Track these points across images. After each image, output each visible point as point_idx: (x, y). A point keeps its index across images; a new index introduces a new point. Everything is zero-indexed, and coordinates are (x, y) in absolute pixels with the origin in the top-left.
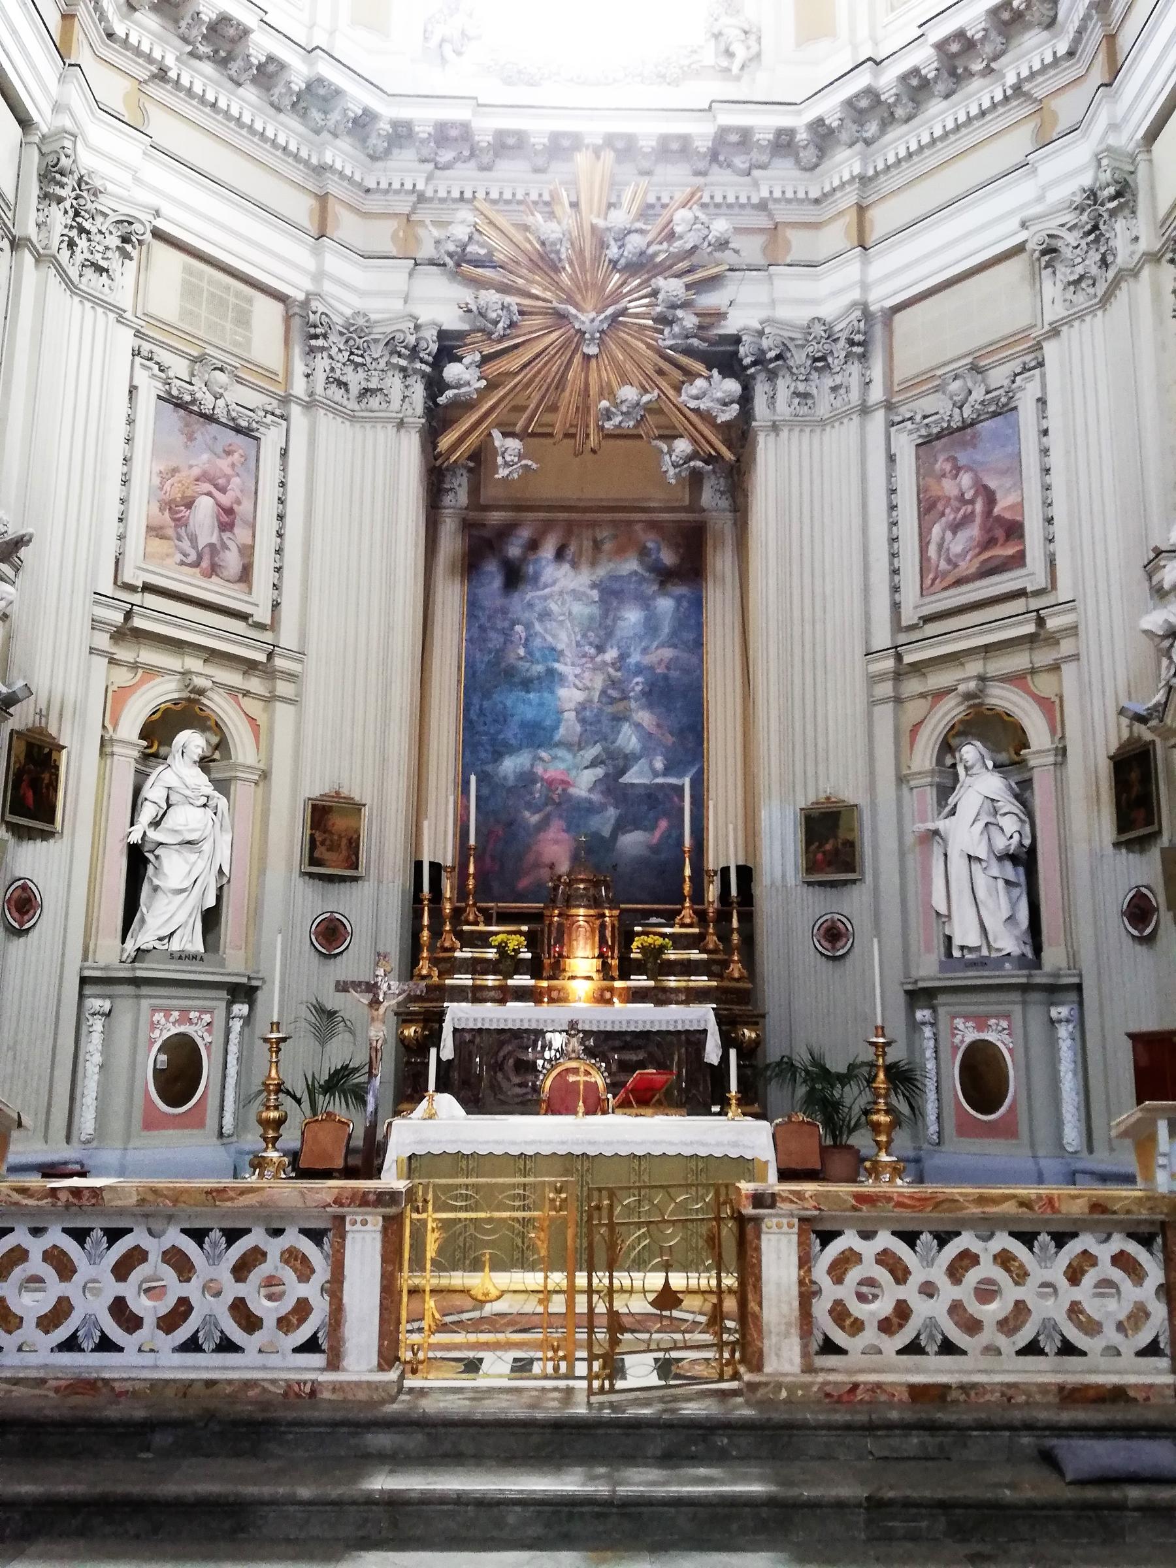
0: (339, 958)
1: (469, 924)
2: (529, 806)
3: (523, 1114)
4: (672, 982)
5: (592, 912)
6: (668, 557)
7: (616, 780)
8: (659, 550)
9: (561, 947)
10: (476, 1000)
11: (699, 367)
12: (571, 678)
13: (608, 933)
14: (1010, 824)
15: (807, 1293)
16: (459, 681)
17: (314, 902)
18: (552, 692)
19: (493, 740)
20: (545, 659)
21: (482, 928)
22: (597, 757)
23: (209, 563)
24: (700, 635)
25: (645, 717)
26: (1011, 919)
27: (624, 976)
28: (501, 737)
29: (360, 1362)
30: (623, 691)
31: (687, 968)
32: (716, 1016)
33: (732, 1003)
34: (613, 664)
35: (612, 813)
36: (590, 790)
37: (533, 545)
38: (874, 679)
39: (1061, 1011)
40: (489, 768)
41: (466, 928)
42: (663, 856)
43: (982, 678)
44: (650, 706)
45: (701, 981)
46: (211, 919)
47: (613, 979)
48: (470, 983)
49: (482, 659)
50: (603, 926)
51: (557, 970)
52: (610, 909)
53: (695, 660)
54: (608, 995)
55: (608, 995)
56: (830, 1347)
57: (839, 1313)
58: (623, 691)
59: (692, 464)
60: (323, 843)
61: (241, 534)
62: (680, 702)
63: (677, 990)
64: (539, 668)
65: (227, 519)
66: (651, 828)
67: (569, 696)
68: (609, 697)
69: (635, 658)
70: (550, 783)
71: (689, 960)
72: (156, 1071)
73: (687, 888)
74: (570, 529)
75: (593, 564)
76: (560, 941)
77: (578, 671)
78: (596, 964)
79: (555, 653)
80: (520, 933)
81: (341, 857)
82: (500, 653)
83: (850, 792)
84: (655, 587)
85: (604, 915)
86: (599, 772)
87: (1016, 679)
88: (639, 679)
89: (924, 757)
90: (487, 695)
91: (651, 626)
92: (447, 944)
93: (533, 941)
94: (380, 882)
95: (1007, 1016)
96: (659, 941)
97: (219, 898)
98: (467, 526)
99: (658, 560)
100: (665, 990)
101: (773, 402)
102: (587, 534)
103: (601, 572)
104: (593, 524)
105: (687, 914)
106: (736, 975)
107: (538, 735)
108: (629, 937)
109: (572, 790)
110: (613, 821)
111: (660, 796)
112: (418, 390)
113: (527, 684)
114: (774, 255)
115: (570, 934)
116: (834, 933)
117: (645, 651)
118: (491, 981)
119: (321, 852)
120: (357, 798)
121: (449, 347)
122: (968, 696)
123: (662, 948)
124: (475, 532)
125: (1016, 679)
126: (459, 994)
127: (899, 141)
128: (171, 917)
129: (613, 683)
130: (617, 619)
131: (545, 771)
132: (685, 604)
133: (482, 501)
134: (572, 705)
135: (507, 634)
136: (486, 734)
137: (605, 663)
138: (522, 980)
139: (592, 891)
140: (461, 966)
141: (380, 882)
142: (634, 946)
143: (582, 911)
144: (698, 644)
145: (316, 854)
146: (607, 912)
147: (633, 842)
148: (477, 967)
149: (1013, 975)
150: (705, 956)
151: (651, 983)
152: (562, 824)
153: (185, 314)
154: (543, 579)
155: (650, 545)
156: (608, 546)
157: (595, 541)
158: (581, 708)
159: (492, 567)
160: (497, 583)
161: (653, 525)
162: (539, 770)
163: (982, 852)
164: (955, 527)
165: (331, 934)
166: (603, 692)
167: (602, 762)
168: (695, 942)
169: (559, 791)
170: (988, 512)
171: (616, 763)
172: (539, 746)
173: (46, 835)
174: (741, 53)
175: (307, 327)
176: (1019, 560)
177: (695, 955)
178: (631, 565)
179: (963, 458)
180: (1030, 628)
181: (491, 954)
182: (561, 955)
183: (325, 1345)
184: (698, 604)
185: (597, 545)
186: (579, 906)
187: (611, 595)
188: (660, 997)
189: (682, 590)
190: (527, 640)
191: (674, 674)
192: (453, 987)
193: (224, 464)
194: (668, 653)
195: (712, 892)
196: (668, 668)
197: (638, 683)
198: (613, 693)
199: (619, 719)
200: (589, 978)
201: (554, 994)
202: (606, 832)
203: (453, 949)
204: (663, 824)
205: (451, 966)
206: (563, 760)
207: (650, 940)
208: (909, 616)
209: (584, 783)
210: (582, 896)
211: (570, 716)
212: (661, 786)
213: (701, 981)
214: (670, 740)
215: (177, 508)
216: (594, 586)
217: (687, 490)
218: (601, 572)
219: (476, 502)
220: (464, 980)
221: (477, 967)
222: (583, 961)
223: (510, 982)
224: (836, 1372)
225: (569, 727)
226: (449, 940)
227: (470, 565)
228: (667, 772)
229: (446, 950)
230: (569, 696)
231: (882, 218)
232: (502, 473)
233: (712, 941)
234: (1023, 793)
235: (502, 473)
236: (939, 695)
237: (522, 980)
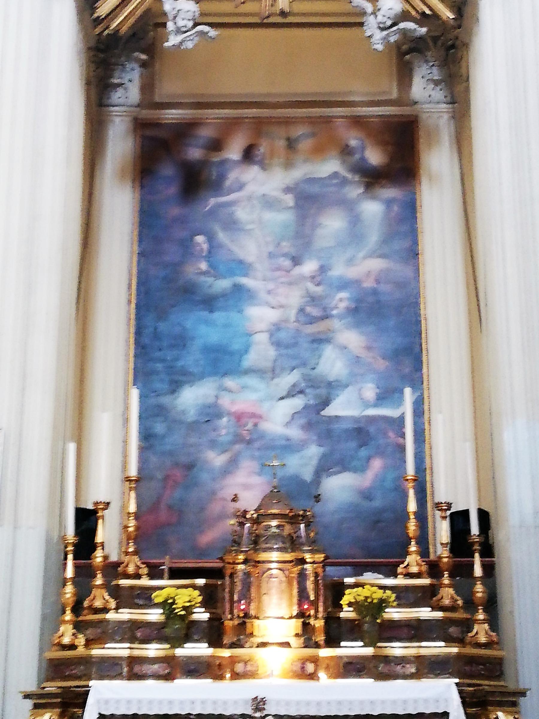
1: (127, 576)
2: (213, 444)
4: (396, 649)
5: (288, 557)
6: (375, 157)
7: (318, 413)
8: (363, 148)
9: (248, 604)
10: (134, 676)
12: (263, 295)
13: (310, 585)
16: (130, 302)
18: (240, 311)
19: (171, 369)
20: (231, 273)
21: (145, 582)
22: (294, 385)
24: (415, 242)
25: (352, 338)
27: (332, 641)
28: (180, 364)
30: (325, 309)
31: (416, 631)
32: (461, 692)
33: (479, 676)
34: (313, 277)
35: (314, 451)
36: (288, 424)
37: (216, 145)
40: (165, 400)
41: (124, 582)
42: (377, 503)
44: (357, 325)
45: (435, 648)
47: (317, 646)
48: (125, 653)
49: (315, 646)
50: (302, 576)
51: (243, 632)
52: (311, 551)
53: (408, 272)
54: (310, 668)
55: (310, 668)
58: (325, 309)
59: (402, 25)
62: (395, 320)
63: (402, 660)
64: (223, 284)
66: (362, 469)
68: (308, 315)
69: (339, 270)
70: (239, 417)
71: (419, 621)
73: (412, 526)
74: (259, 126)
75: (288, 165)
76: (246, 595)
77: (271, 286)
78: (296, 625)
79: (243, 267)
80: (194, 587)
82: (176, 267)
84: (361, 190)
85: (303, 561)
86: (298, 402)
88: (343, 295)
90: (162, 315)
91: (355, 232)
92: (98, 604)
93: (210, 598)
94: (16, 527)
96: (379, 594)
98: (141, 126)
99: (363, 159)
100: (387, 659)
102: (281, 132)
103: (299, 173)
104: (287, 122)
105: (413, 561)
106: (483, 639)
107: (223, 361)
108: (337, 590)
109: (265, 426)
110: (315, 462)
111: (372, 430)
113: (210, 302)
115: (259, 587)
117: (350, 262)
118: (153, 650)
123: (382, 604)
124: (149, 133)
126: (110, 669)
129: (313, 299)
130: (315, 226)
131: (233, 402)
132: (396, 208)
133: (157, 99)
134: (263, 326)
135: (186, 245)
136: (163, 361)
137: (303, 278)
138: (198, 649)
139: (288, 529)
140: (115, 633)
141: (16, 527)
142: (344, 601)
143: (275, 556)
144: (413, 254)
146: (308, 557)
147: (340, 488)
148: (134, 632)
150: (439, 615)
151: (369, 651)
152: (254, 465)
154: (228, 183)
155: (353, 143)
156: (305, 145)
157: (288, 139)
158: (276, 328)
159: (168, 170)
160: (172, 190)
161: (358, 122)
162: (226, 402)
166: (302, 310)
167: (301, 392)
168: (426, 596)
169: (250, 426)
171: (321, 392)
172: (225, 374)
177: (425, 613)
178: (331, 166)
181: (155, 615)
182: (247, 615)
184: (410, 212)
185: (291, 144)
186: (271, 549)
187: (308, 201)
188: (378, 668)
189: (390, 192)
190: (210, 252)
191: (384, 288)
192: (103, 660)
194: (376, 264)
195: (443, 531)
196: (378, 281)
197: (342, 300)
198: (315, 312)
199: (320, 341)
200: (287, 645)
201: (239, 668)
202: (308, 475)
203: (105, 610)
204: (377, 464)
205: (103, 633)
206: (255, 390)
207: (362, 593)
210: (275, 536)
211: (262, 338)
212: (372, 420)
213: (435, 648)
214: (382, 365)
216: (288, 190)
217: (395, 84)
218: (299, 173)
219: (149, 99)
220: (119, 650)
221: (134, 632)
222: (276, 617)
223: (179, 652)
225: (261, 352)
226: (100, 597)
227: (144, 169)
229: (97, 611)
230: (260, 316)
232: (173, 40)
233: (447, 594)
235: (173, 40)
237: (198, 649)
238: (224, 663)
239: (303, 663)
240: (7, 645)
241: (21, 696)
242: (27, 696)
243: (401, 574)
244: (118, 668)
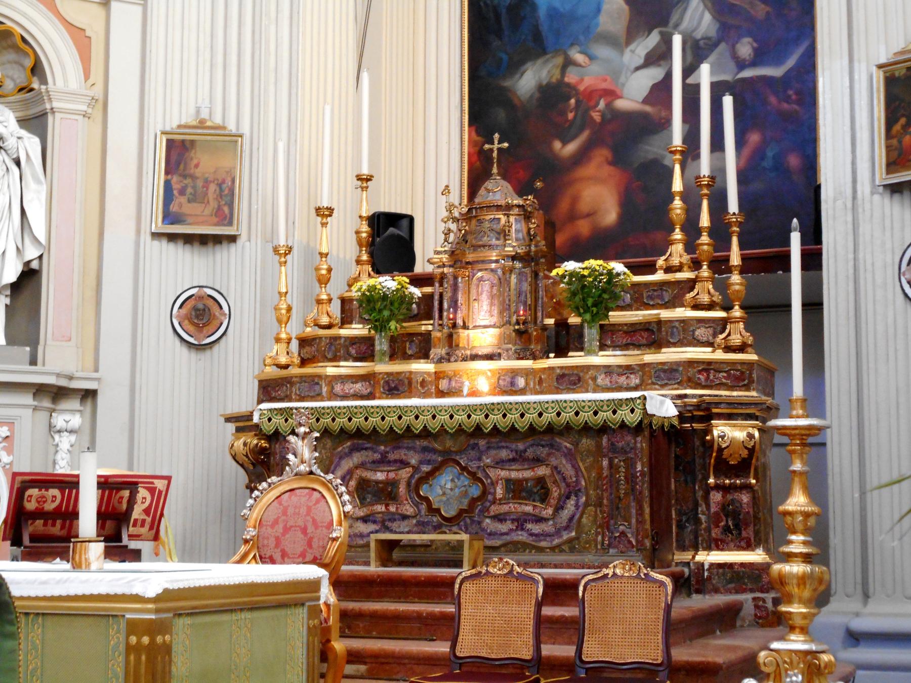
0: (216, 348)
60: (182, 192)
81: (207, 211)
105: (677, 252)
119: (180, 204)
120: (232, 127)
145: (174, 208)
165: (201, 318)
228: (758, 59)
238: (428, 379)
239: (513, 378)
240: (290, 606)
241: (222, 419)
242: (228, 420)
243: (661, 268)
244: (317, 388)
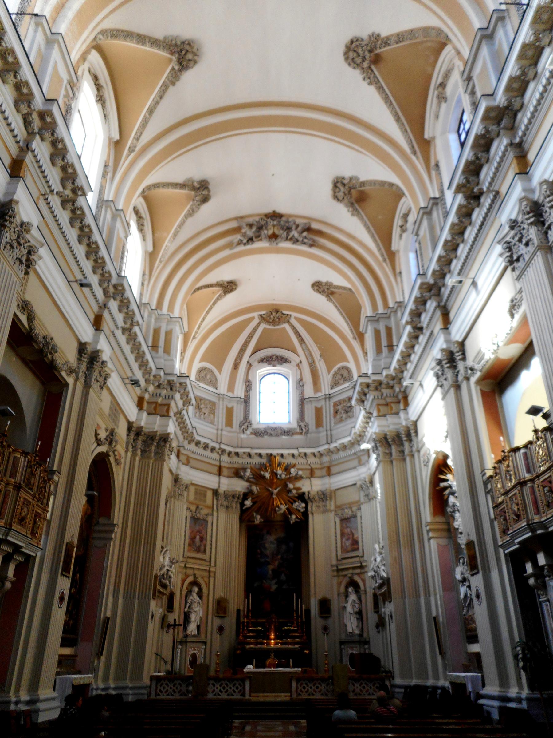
3: (241, 309)
11: (296, 500)
14: (357, 605)
15: (297, 688)
17: (217, 622)
23: (198, 550)
26: (357, 627)
29: (247, 697)
31: (294, 637)
38: (333, 571)
39: (367, 646)
43: (352, 574)
46: (198, 627)
56: (300, 695)
57: (301, 691)
61: (204, 541)
64: (263, 560)
65: (202, 539)
67: (271, 567)
72: (190, 660)
83: (329, 597)
87: (358, 574)
89: (342, 590)
95: (356, 647)
97: (200, 623)
101: (313, 507)
112: (239, 506)
114: (312, 474)
116: (325, 629)
121: (246, 496)
122: (350, 577)
125: (358, 574)
127: (335, 457)
128: (192, 628)
149: (357, 638)
153: (195, 499)
158: (273, 570)
163: (352, 612)
164: (348, 539)
165: (221, 629)
170: (353, 538)
173: (172, 612)
174: (304, 430)
175: (215, 492)
176: (358, 549)
179: (348, 525)
180: (359, 565)
183: (243, 694)
193: (201, 528)
205: (246, 637)
208: (339, 558)
209: (274, 587)
211: (270, 572)
213: (297, 640)
215: (193, 539)
224: (300, 697)
231: (334, 470)
234: (360, 599)
236: (345, 576)
